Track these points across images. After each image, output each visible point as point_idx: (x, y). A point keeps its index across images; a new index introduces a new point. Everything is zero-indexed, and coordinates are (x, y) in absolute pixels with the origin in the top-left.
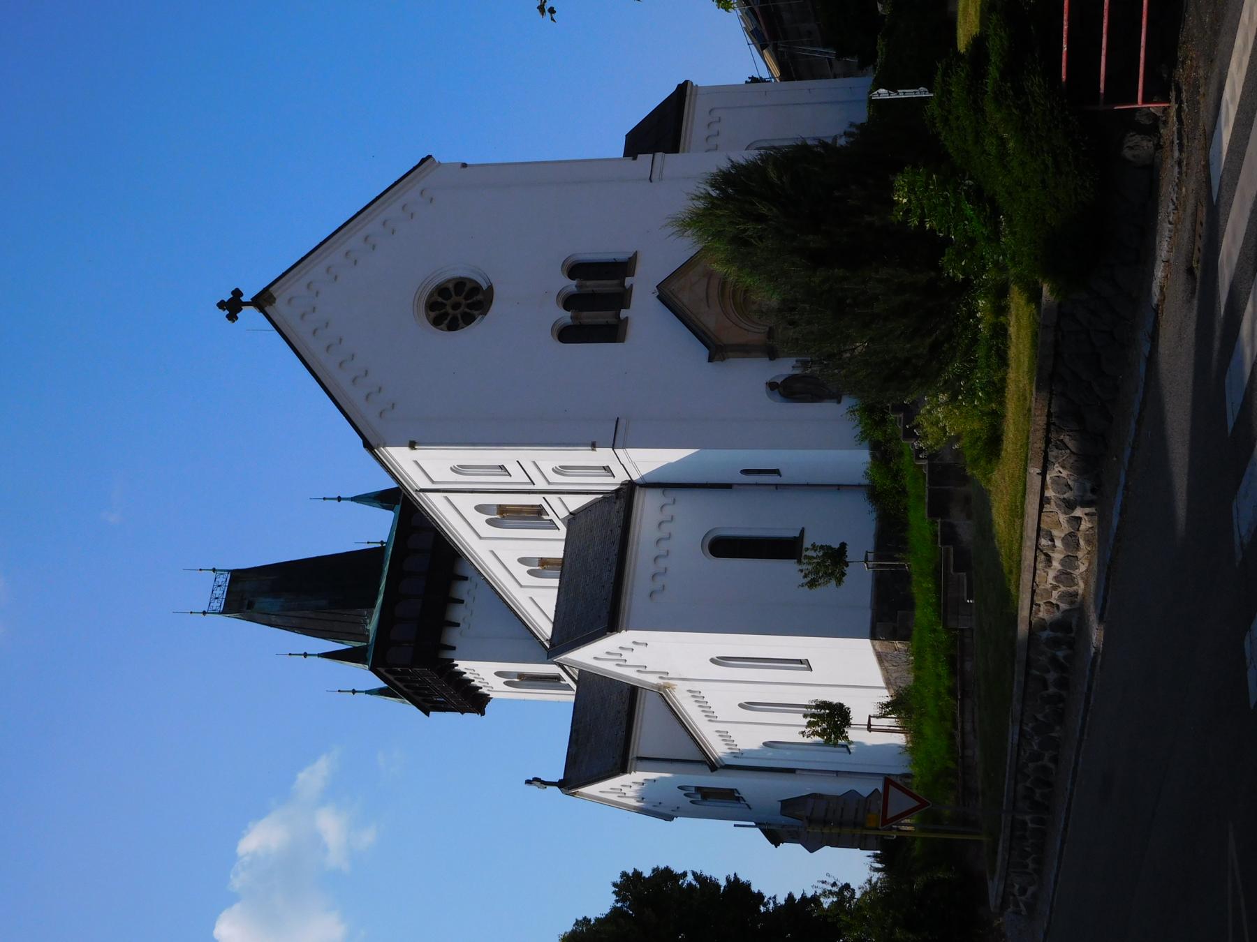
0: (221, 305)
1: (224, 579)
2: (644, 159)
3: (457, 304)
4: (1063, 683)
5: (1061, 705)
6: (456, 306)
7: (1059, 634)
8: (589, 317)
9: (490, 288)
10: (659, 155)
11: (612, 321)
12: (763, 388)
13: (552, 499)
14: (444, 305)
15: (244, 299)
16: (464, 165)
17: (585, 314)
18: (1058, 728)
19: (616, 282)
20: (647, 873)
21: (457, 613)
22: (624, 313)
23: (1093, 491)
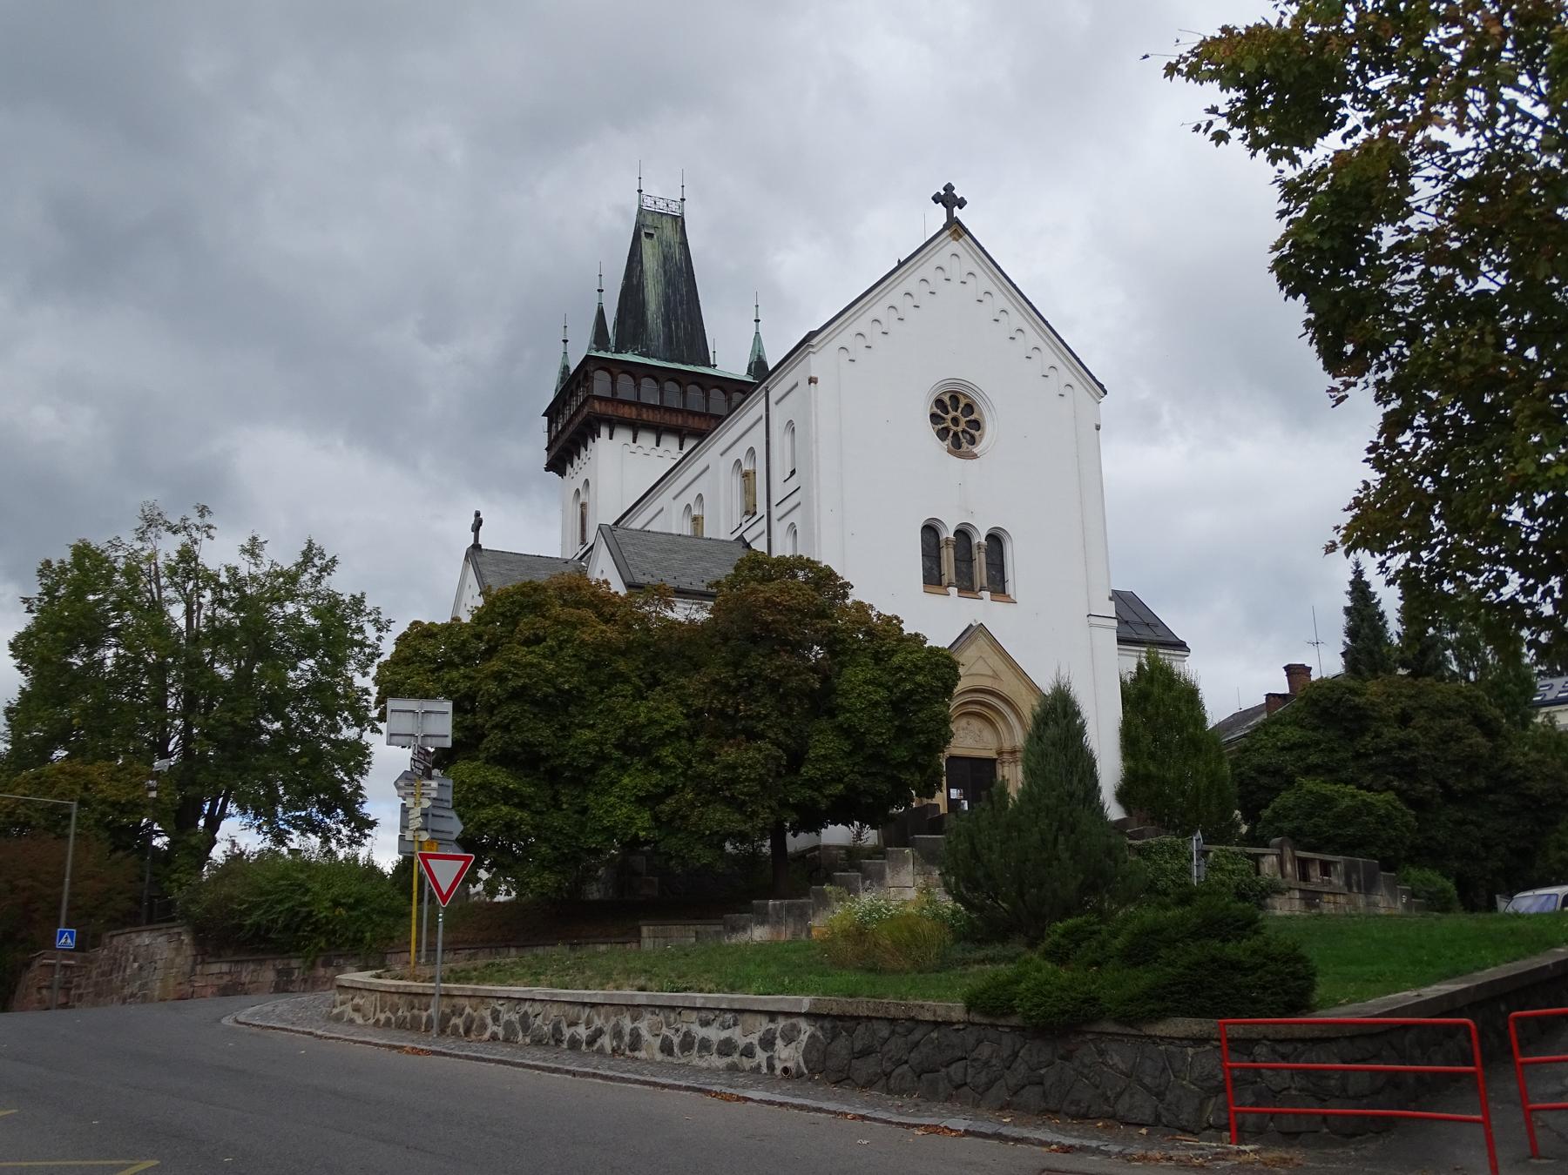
0: (949, 188)
1: (674, 209)
2: (1110, 609)
3: (957, 419)
4: (574, 1044)
5: (552, 1042)
6: (955, 421)
7: (627, 1039)
8: (948, 556)
9: (975, 456)
10: (1115, 623)
11: (945, 580)
13: (763, 524)
14: (956, 434)
15: (957, 211)
16: (1098, 428)
17: (951, 551)
18: (528, 1040)
21: (647, 440)
23: (786, 1070)
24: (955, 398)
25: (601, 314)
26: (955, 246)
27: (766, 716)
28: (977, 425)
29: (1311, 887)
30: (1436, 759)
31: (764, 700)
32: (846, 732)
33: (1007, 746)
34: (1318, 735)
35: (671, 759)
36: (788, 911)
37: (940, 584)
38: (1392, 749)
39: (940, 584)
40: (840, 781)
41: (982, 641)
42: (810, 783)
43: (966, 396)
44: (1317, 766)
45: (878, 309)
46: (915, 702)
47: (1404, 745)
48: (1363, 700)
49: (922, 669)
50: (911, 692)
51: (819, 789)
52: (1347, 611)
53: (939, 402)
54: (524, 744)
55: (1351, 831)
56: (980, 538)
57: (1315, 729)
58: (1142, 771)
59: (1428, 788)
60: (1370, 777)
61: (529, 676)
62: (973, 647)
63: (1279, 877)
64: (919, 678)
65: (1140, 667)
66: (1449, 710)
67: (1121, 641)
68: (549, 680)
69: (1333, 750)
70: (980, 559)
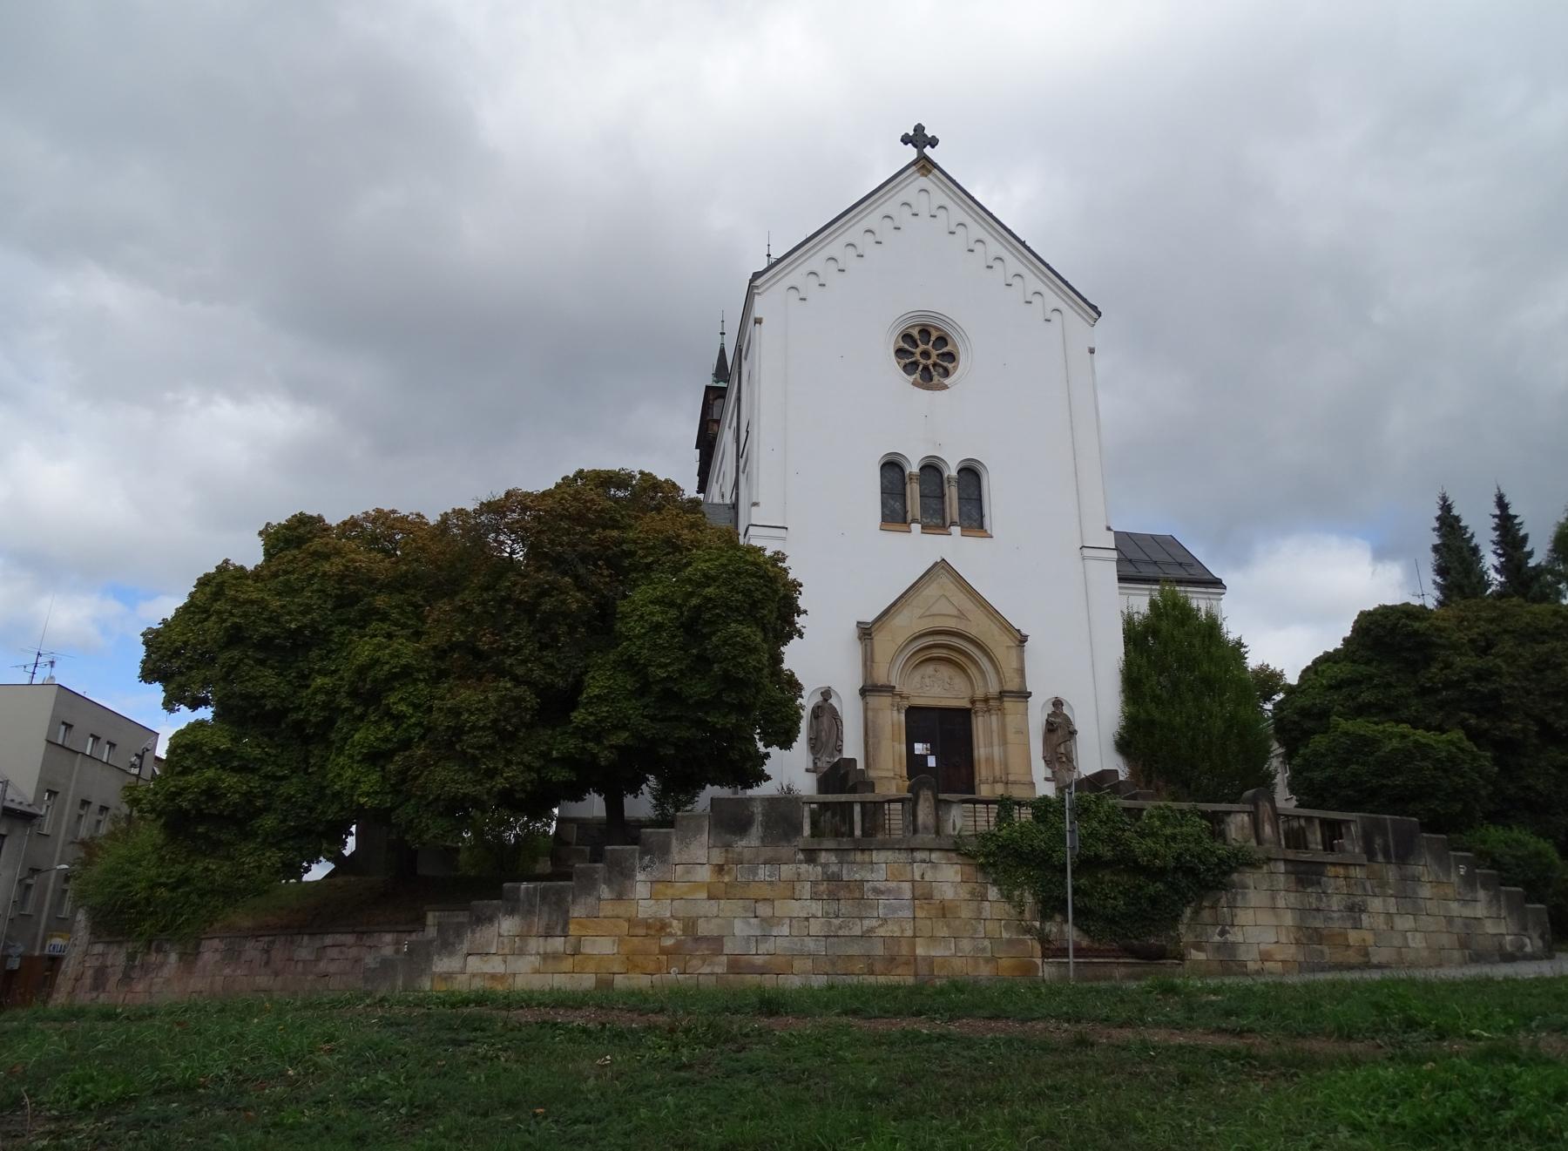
0: (919, 129)
3: (927, 353)
6: (926, 354)
8: (914, 491)
9: (946, 387)
10: (1114, 554)
11: (909, 518)
12: (825, 685)
14: (926, 368)
15: (928, 150)
16: (1092, 351)
19: (956, 518)
20: (1253, 662)
22: (956, 530)
24: (925, 332)
25: (722, 351)
26: (923, 182)
27: (518, 650)
28: (951, 357)
29: (1305, 856)
30: (1528, 693)
31: (516, 629)
32: (629, 664)
33: (979, 694)
34: (1372, 670)
35: (403, 707)
36: (544, 898)
37: (905, 521)
38: (1465, 681)
39: (905, 521)
40: (624, 727)
41: (945, 580)
42: (584, 732)
43: (937, 329)
44: (1370, 705)
45: (835, 247)
46: (709, 623)
47: (1480, 676)
48: (1426, 624)
49: (715, 579)
50: (698, 608)
51: (598, 739)
52: (1436, 549)
53: (907, 337)
54: (246, 697)
55: (1399, 780)
56: (951, 471)
57: (1368, 662)
58: (1143, 716)
59: (1517, 726)
60: (1439, 716)
61: (245, 615)
62: (934, 585)
63: (1253, 842)
64: (709, 591)
65: (1153, 604)
66: (1544, 632)
67: (1121, 579)
68: (273, 620)
69: (1389, 685)
70: (952, 493)
